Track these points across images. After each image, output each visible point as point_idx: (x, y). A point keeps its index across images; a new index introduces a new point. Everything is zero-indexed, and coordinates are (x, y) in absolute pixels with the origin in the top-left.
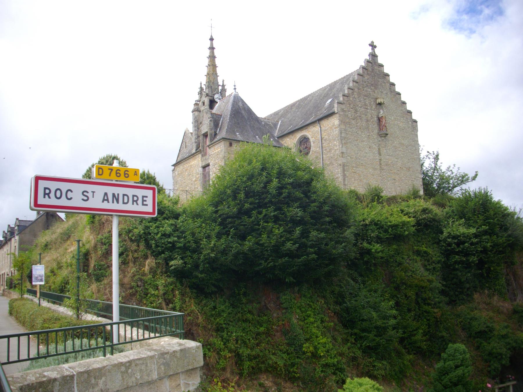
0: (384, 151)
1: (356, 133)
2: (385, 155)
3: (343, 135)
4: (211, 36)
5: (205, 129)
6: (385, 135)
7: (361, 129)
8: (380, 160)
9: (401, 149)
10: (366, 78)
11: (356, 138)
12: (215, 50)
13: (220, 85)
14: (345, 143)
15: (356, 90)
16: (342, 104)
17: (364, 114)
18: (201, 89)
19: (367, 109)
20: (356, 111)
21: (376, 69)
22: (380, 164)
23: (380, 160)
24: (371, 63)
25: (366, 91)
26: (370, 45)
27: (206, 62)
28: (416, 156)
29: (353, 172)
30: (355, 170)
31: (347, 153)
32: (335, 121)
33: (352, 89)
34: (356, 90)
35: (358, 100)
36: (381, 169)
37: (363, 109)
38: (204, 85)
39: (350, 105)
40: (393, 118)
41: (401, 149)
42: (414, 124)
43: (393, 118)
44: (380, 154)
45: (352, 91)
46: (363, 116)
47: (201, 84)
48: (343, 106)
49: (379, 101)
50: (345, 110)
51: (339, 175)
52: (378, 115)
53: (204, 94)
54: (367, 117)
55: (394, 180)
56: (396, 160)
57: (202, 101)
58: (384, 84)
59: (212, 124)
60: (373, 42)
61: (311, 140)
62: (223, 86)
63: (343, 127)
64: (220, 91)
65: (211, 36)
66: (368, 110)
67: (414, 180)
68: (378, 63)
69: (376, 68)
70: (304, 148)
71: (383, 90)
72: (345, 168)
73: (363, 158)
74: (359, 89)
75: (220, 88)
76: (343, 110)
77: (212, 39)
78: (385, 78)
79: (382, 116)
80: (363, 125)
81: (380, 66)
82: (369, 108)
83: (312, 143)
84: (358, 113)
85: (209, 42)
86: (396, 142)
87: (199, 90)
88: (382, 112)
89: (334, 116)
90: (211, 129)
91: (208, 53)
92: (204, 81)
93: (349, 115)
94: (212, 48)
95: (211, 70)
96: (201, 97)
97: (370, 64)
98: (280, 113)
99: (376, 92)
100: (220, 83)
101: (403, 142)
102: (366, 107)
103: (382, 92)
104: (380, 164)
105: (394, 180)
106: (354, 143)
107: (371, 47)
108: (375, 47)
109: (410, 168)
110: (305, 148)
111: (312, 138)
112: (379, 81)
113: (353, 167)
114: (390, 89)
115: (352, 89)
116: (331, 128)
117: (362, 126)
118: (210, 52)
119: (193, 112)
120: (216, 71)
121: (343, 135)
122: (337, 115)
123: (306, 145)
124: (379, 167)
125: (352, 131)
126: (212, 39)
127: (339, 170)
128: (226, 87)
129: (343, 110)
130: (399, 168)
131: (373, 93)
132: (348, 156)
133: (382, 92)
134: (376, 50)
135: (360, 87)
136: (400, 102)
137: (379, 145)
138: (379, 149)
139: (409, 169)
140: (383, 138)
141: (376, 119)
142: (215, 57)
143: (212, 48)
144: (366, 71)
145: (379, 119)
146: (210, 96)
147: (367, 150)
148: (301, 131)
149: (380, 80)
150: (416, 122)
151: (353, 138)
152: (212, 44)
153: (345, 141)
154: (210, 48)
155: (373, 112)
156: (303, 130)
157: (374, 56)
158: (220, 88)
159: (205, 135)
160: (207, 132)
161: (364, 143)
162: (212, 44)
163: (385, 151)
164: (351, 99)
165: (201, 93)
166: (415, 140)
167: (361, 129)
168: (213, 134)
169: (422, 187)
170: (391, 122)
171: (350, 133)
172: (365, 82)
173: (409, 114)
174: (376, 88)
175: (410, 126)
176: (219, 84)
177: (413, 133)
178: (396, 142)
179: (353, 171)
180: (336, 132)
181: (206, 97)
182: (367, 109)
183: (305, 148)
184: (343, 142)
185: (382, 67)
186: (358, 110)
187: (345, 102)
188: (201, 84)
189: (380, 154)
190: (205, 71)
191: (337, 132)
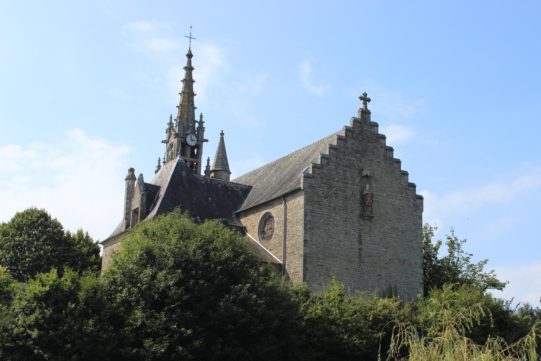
0: (366, 238)
1: (328, 215)
2: (367, 243)
3: (308, 218)
4: (190, 51)
5: (136, 203)
6: (368, 218)
7: (335, 209)
8: (361, 249)
9: (394, 236)
10: (350, 142)
11: (326, 222)
12: (193, 72)
13: (197, 121)
14: (310, 229)
15: (333, 159)
16: (311, 178)
17: (341, 191)
18: (171, 124)
19: (347, 183)
20: (330, 187)
21: (366, 131)
22: (360, 255)
23: (361, 249)
24: (360, 123)
25: (348, 160)
26: (361, 98)
27: (180, 87)
28: (416, 245)
29: (319, 265)
30: (321, 263)
31: (311, 241)
32: (300, 200)
33: (327, 159)
34: (333, 159)
35: (335, 173)
36: (361, 261)
37: (341, 184)
38: (175, 120)
39: (322, 178)
40: (385, 195)
41: (394, 236)
42: (418, 201)
43: (385, 195)
44: (360, 242)
45: (326, 161)
46: (340, 193)
47: (171, 117)
48: (312, 181)
49: (365, 173)
50: (314, 185)
51: (300, 268)
52: (363, 192)
53: (173, 133)
54: (346, 194)
55: (379, 276)
56: (385, 250)
57: (170, 143)
58: (376, 150)
59: (145, 199)
60: (365, 95)
61: (276, 219)
62: (201, 123)
63: (310, 208)
64: (196, 129)
65: (190, 51)
66: (348, 185)
67: (410, 276)
68: (370, 122)
69: (366, 129)
70: (268, 229)
71: (373, 158)
72: (308, 260)
73: (334, 248)
74: (337, 157)
75: (197, 125)
76: (311, 187)
77: (190, 56)
78: (379, 141)
79: (367, 194)
80: (339, 204)
81: (372, 125)
82: (350, 182)
83: (276, 223)
84: (333, 189)
85: (186, 59)
86: (386, 226)
87: (167, 127)
88: (368, 186)
89: (300, 193)
90: (142, 205)
91: (183, 74)
92: (176, 113)
93: (320, 192)
94: (189, 69)
95: (186, 99)
96: (169, 138)
97: (358, 124)
98: (259, 174)
99: (363, 161)
100: (197, 118)
101: (398, 226)
102: (347, 181)
103: (372, 161)
104: (360, 255)
105: (379, 276)
106: (323, 228)
107: (362, 101)
108: (369, 100)
109: (404, 260)
110: (270, 229)
111: (276, 217)
112: (369, 146)
113: (319, 259)
114: (385, 156)
115: (327, 159)
116: (295, 207)
117: (338, 205)
118: (187, 74)
119: (126, 180)
120: (193, 102)
121: (308, 218)
122: (303, 192)
123: (270, 226)
124: (357, 260)
125: (321, 213)
126: (190, 56)
127: (300, 262)
128: (204, 125)
129: (311, 187)
130: (388, 260)
131: (359, 162)
132: (313, 245)
133: (372, 161)
134: (369, 105)
135: (340, 156)
136: (398, 173)
137: (361, 230)
138: (360, 236)
139: (403, 262)
140: (367, 222)
141: (359, 196)
142: (193, 81)
143: (189, 69)
144: (350, 134)
145: (363, 197)
146: (180, 137)
147: (342, 237)
148: (293, 196)
149: (371, 145)
150: (421, 198)
151: (322, 221)
152: (189, 62)
153: (310, 226)
154: (185, 68)
155: (355, 187)
156: (268, 206)
157: (365, 113)
158: (197, 125)
159: (136, 211)
160: (138, 208)
161: (338, 228)
162: (189, 62)
163: (369, 238)
164: (325, 171)
165: (170, 130)
166: (417, 224)
167: (335, 209)
168: (145, 211)
169: (423, 286)
170: (381, 200)
171: (319, 215)
172: (348, 149)
173: (411, 188)
174: (362, 155)
175: (411, 204)
176: (196, 119)
177: (415, 213)
178: (386, 226)
179: (319, 264)
180: (301, 213)
181: (175, 138)
182: (347, 183)
183: (270, 229)
184: (308, 227)
185: (376, 128)
186: (334, 185)
187: (315, 175)
188: (171, 117)
189: (360, 242)
190: (178, 100)
191: (301, 214)
